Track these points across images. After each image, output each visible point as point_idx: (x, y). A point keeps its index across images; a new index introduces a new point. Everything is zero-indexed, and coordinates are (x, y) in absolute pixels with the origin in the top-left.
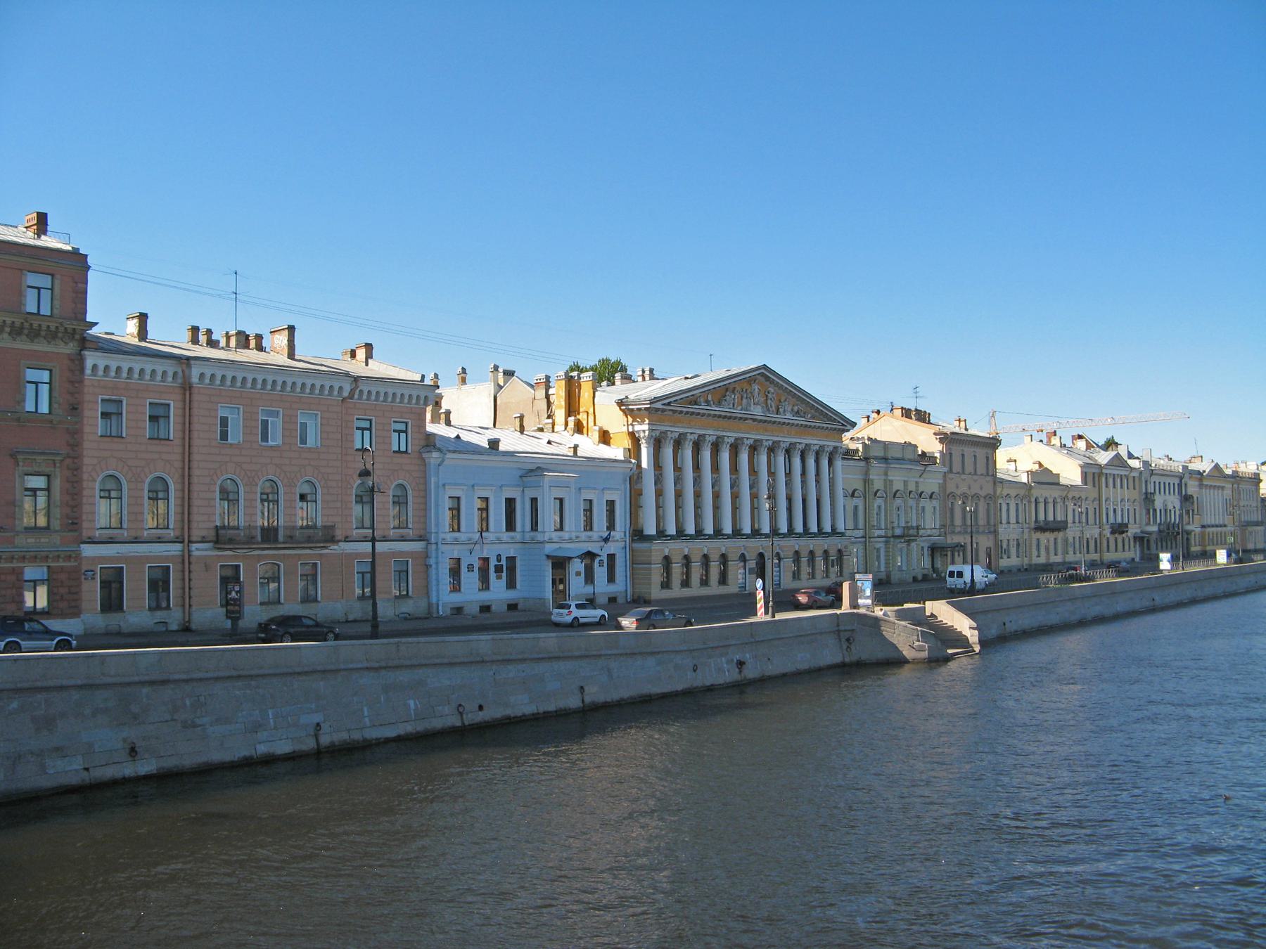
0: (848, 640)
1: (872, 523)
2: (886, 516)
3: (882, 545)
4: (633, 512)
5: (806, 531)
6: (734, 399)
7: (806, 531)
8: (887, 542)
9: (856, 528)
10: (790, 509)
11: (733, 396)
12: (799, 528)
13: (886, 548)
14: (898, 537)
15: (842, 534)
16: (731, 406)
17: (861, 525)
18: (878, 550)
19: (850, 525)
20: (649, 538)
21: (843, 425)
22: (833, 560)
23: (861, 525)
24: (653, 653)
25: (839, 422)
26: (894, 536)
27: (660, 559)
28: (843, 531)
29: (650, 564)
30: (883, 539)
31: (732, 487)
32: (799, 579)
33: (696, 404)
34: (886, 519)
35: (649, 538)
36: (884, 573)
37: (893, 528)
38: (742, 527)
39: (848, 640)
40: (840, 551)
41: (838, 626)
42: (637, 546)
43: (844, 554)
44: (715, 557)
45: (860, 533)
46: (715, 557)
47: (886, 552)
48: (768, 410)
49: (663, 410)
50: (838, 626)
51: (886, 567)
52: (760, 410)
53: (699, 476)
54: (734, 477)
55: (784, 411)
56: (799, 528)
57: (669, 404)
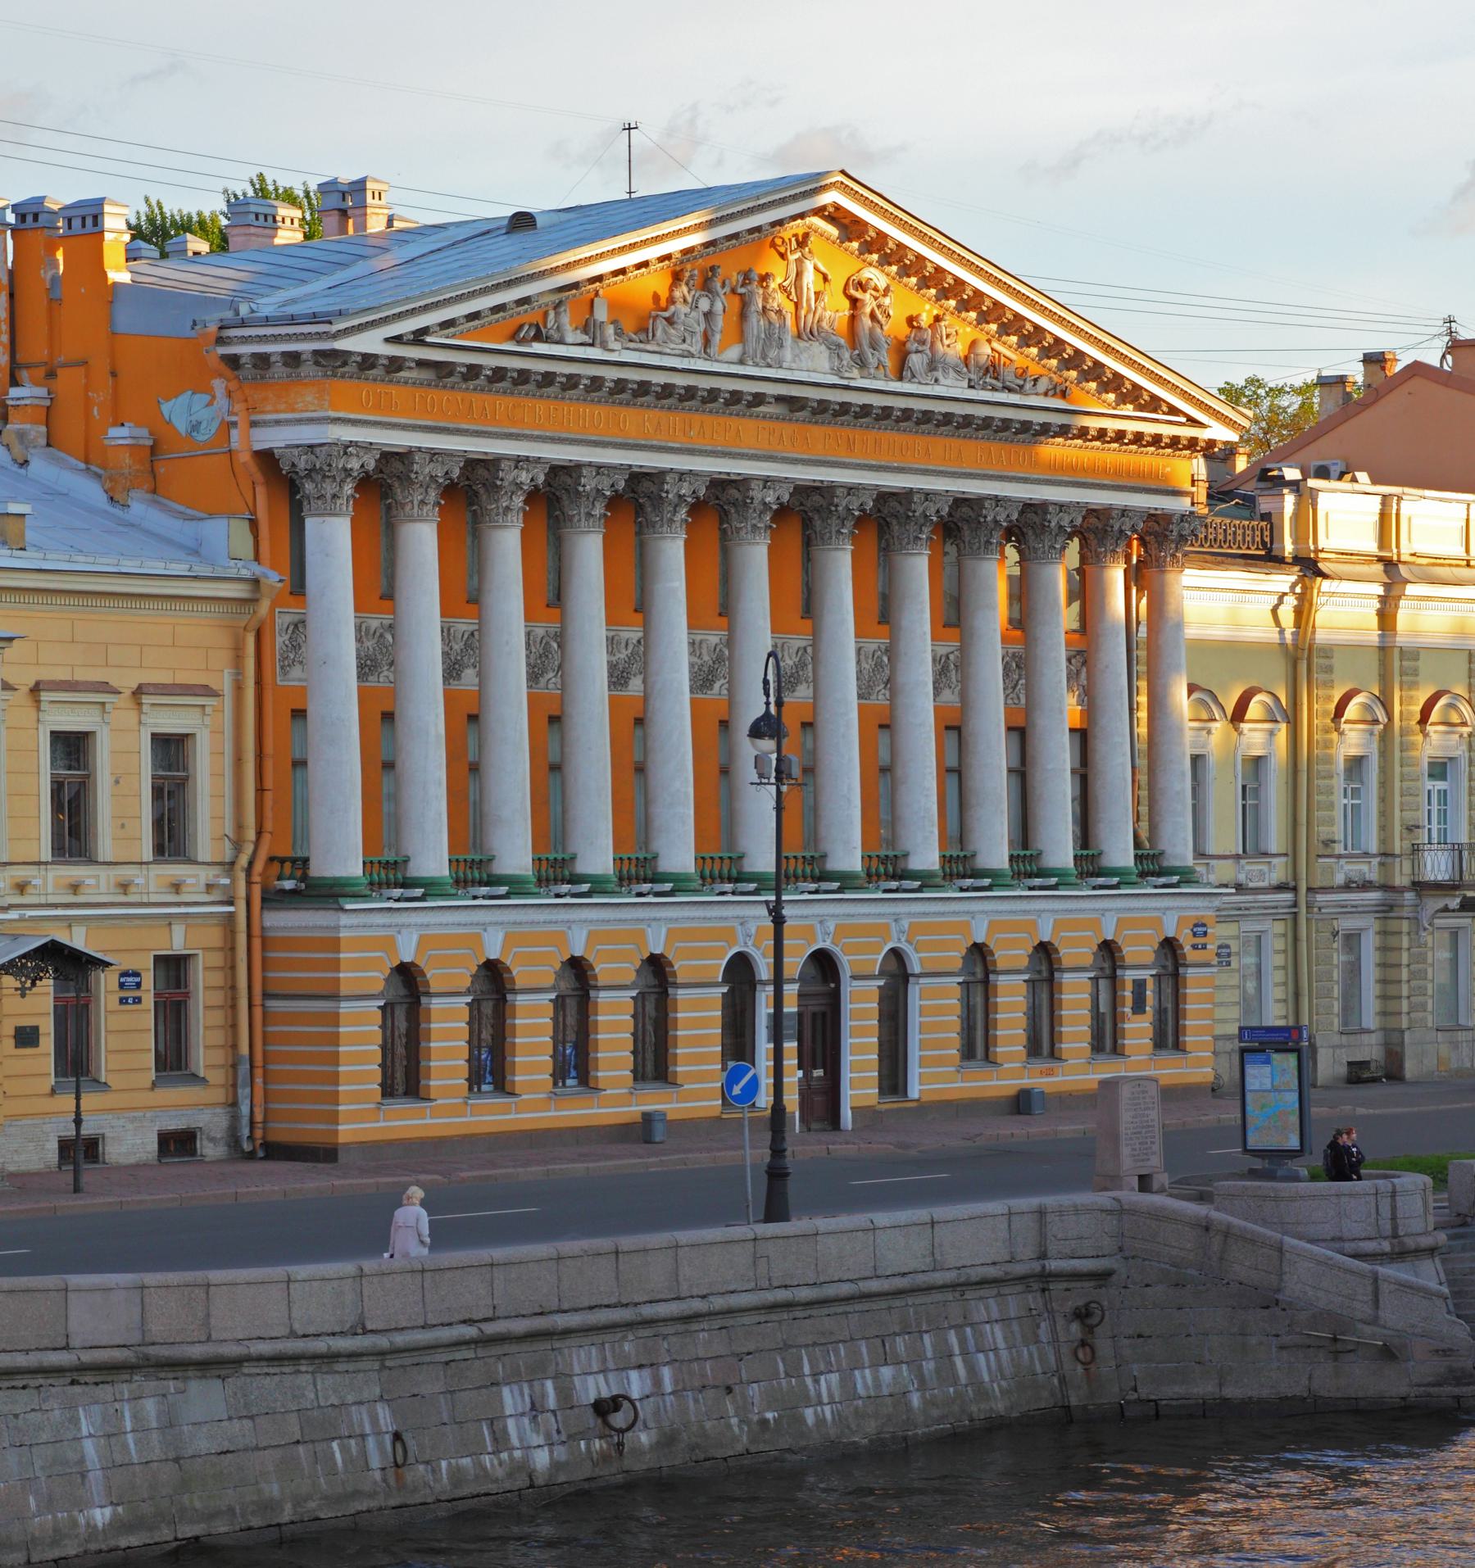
0: (1082, 1315)
1: (1323, 831)
2: (1385, 800)
3: (1369, 926)
4: (269, 783)
5: (1090, 865)
6: (708, 315)
7: (1090, 865)
8: (1386, 910)
9: (1252, 848)
10: (1022, 774)
11: (704, 304)
12: (995, 851)
13: (1384, 933)
14: (1438, 887)
15: (1186, 877)
16: (696, 346)
17: (1275, 838)
18: (1352, 940)
19: (1224, 835)
20: (329, 893)
21: (1193, 422)
22: (1140, 986)
23: (1275, 838)
24: (207, 1366)
25: (1173, 410)
26: (1420, 887)
27: (377, 978)
28: (1190, 861)
29: (335, 997)
30: (1374, 896)
31: (452, 671)
32: (1117, 1050)
33: (538, 337)
34: (1385, 814)
35: (329, 893)
36: (1374, 1039)
37: (1416, 850)
38: (1104, 847)
39: (1082, 1315)
40: (1170, 945)
41: (1043, 1256)
42: (285, 921)
43: (1191, 955)
44: (1012, 954)
45: (1278, 871)
46: (1012, 954)
47: (1383, 949)
48: (861, 363)
49: (396, 364)
50: (1043, 1256)
51: (1384, 1013)
52: (826, 366)
53: (561, 638)
54: (463, 626)
55: (932, 366)
56: (1060, 849)
57: (418, 337)
